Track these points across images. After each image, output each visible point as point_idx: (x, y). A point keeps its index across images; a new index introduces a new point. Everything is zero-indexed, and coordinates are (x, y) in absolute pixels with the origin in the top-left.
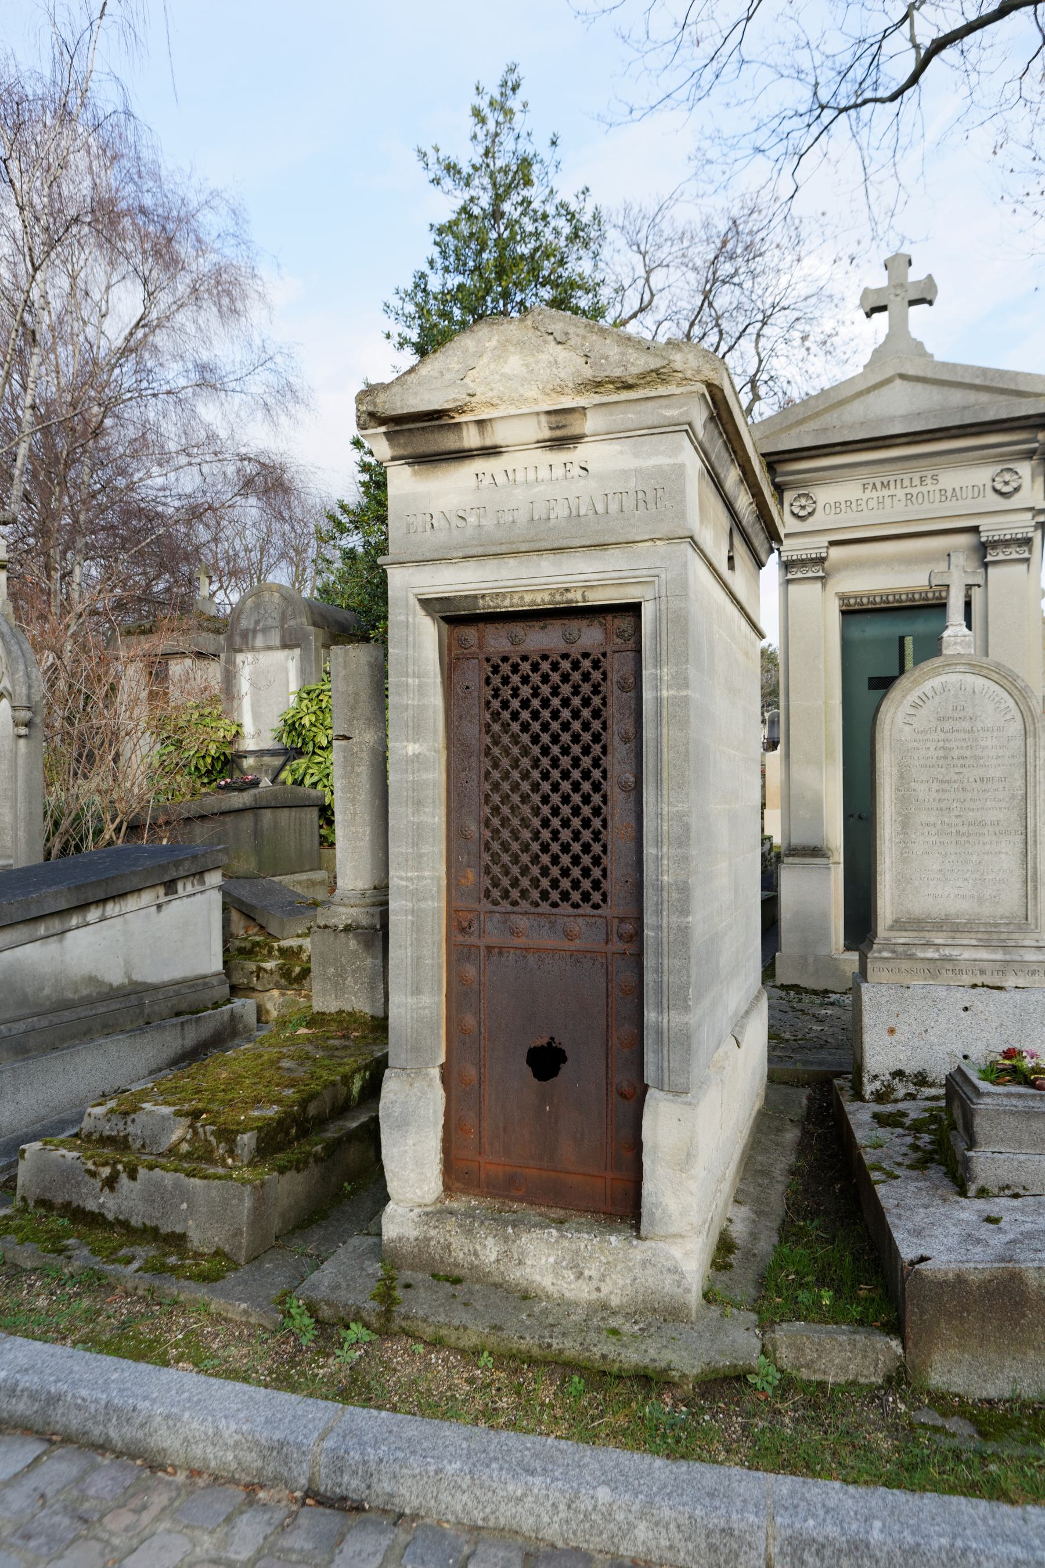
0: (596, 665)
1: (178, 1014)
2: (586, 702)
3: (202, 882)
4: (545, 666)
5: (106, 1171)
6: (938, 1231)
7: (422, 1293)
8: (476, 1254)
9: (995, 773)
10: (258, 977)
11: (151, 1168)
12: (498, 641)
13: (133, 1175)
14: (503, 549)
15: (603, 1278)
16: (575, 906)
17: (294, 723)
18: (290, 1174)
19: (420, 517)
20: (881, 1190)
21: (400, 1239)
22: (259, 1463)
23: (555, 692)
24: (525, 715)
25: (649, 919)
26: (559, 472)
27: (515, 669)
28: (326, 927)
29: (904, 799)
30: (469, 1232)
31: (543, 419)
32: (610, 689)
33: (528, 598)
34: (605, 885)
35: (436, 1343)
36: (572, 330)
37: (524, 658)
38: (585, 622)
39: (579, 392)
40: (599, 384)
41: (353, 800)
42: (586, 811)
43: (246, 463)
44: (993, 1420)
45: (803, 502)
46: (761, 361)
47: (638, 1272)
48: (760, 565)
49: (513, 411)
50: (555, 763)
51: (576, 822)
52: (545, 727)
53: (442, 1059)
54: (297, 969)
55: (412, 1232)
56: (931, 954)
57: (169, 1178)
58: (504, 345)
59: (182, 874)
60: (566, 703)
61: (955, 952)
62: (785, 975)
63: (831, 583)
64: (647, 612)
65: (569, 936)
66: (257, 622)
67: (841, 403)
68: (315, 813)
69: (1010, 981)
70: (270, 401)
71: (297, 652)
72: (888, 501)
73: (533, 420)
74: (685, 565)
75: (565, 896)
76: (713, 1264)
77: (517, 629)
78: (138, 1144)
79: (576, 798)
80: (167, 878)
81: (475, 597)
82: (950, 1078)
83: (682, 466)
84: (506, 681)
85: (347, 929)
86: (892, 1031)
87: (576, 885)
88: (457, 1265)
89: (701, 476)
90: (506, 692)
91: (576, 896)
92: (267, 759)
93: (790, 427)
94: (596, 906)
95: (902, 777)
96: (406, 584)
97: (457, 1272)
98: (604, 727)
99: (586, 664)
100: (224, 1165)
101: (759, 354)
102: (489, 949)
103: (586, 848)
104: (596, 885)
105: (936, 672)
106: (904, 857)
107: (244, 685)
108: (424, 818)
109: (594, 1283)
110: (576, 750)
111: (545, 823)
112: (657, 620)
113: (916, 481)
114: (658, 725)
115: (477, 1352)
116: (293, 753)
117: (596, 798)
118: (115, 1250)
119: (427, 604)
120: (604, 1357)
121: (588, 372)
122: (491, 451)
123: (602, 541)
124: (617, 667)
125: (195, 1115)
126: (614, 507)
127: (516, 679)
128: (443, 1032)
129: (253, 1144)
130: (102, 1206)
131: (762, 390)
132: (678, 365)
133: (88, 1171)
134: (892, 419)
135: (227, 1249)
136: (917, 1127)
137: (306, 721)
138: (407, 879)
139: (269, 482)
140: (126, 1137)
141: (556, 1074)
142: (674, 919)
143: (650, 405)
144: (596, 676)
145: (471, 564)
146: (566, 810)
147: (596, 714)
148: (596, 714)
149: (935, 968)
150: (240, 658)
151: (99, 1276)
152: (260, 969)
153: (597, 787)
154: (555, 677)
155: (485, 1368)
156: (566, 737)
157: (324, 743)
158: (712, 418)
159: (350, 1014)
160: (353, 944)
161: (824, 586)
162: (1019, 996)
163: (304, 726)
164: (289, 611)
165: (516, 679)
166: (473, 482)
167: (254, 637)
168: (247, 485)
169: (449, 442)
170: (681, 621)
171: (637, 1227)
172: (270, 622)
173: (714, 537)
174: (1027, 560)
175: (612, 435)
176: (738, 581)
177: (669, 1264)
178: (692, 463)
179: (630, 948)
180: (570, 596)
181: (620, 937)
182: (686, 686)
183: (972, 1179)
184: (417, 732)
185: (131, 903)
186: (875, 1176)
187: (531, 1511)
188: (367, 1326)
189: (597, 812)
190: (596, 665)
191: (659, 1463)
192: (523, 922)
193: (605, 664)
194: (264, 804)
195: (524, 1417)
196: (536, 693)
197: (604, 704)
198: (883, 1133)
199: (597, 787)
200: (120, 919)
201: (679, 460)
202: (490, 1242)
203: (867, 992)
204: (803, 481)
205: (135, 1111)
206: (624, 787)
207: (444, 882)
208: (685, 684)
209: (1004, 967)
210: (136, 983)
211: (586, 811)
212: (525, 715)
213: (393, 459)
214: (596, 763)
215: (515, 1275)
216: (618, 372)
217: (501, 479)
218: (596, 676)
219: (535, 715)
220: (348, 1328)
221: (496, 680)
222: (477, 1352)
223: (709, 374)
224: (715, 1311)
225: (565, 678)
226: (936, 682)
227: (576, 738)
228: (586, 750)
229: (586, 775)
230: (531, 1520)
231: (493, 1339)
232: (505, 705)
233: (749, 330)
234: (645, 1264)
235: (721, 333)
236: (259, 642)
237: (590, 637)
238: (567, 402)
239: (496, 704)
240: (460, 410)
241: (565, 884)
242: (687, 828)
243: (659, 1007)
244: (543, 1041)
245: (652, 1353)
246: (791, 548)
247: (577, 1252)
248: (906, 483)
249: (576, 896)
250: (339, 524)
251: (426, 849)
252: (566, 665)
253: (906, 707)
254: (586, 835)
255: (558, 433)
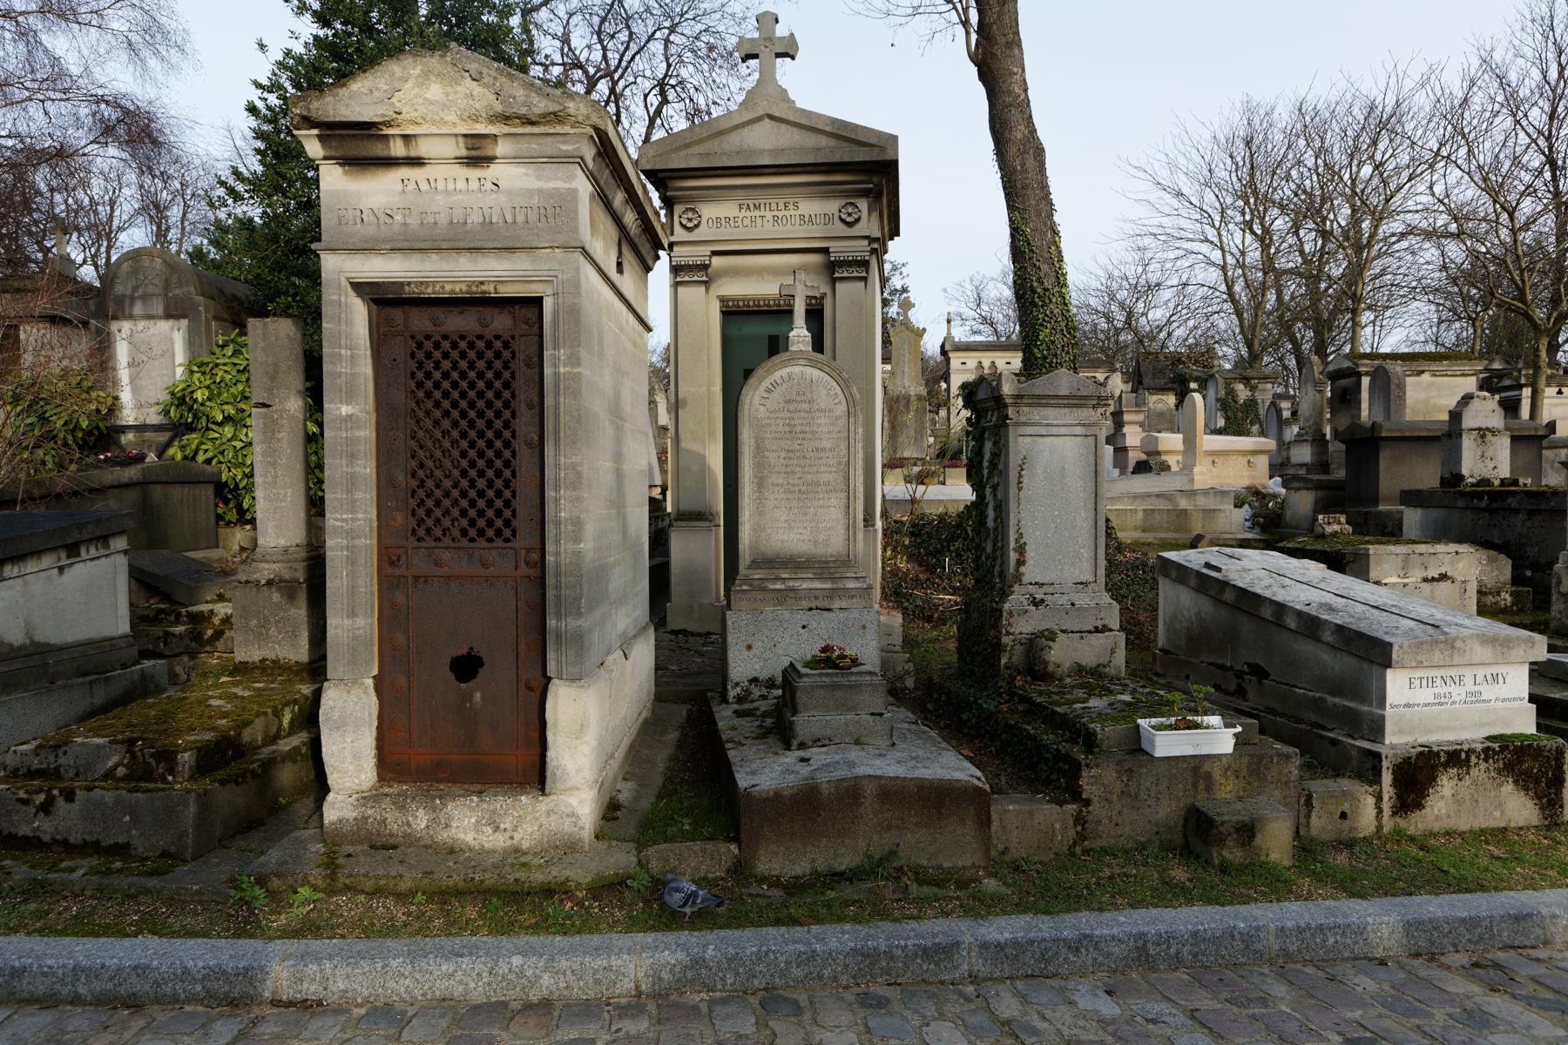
0: (506, 345)
1: (84, 674)
2: (498, 375)
3: (107, 547)
4: (463, 345)
5: (41, 797)
6: (767, 770)
7: (362, 859)
8: (409, 824)
9: (827, 444)
10: (166, 643)
11: (89, 789)
12: (421, 322)
13: (70, 796)
14: (427, 245)
15: (515, 829)
16: (490, 540)
17: (183, 397)
18: (230, 787)
19: (351, 212)
20: (731, 754)
21: (340, 821)
22: (227, 988)
23: (472, 366)
24: (446, 385)
25: (550, 547)
26: (474, 185)
27: (437, 346)
28: (247, 582)
29: (759, 466)
30: (402, 808)
31: (461, 140)
32: (518, 365)
33: (448, 287)
34: (515, 523)
35: (378, 892)
36: (485, 71)
37: (445, 337)
38: (497, 310)
39: (491, 122)
40: (507, 118)
41: (274, 464)
42: (499, 463)
43: (103, 106)
44: (795, 887)
45: (690, 215)
46: (669, 66)
47: (543, 820)
48: (648, 269)
49: (434, 130)
50: (472, 424)
51: (490, 473)
52: (463, 395)
53: (375, 672)
54: (210, 632)
55: (351, 814)
56: (778, 586)
57: (109, 797)
58: (426, 74)
59: (86, 536)
60: (481, 375)
61: (796, 584)
62: (675, 622)
63: (713, 287)
64: (548, 304)
65: (485, 565)
66: (135, 288)
67: (721, 133)
68: (209, 491)
69: (837, 604)
70: (134, 37)
71: (184, 323)
72: (759, 220)
73: (453, 140)
74: (577, 270)
75: (481, 533)
76: (604, 818)
77: (439, 312)
78: (71, 773)
79: (490, 454)
80: (69, 541)
81: (402, 284)
82: (785, 672)
83: (575, 190)
84: (429, 355)
85: (269, 583)
86: (749, 647)
87: (490, 523)
88: (391, 835)
89: (592, 197)
90: (429, 365)
91: (490, 533)
92: (149, 435)
93: (678, 149)
94: (507, 540)
95: (758, 447)
96: (337, 267)
97: (392, 841)
98: (513, 397)
99: (498, 344)
100: (165, 781)
101: (667, 59)
102: (416, 578)
103: (499, 494)
104: (507, 523)
105: (784, 365)
106: (759, 512)
107: (122, 352)
108: (357, 469)
109: (508, 834)
110: (490, 414)
111: (464, 474)
112: (556, 312)
113: (781, 206)
114: (557, 395)
115: (413, 893)
116: (178, 429)
117: (507, 454)
118: (55, 864)
119: (359, 288)
120: (516, 880)
121: (499, 107)
122: (416, 162)
123: (510, 245)
124: (523, 347)
125: (131, 742)
126: (520, 219)
127: (437, 355)
128: (376, 649)
129: (193, 762)
130: (38, 828)
131: (671, 95)
132: (572, 111)
133: (21, 801)
134: (762, 152)
135: (173, 849)
136: (765, 715)
137: (199, 395)
138: (342, 520)
139: (137, 131)
140: (57, 768)
141: (452, 669)
142: (570, 546)
143: (549, 140)
144: (506, 354)
145: (398, 256)
146: (481, 463)
147: (507, 385)
148: (507, 385)
149: (782, 597)
150: (114, 326)
151: (42, 884)
152: (168, 634)
153: (507, 444)
154: (472, 354)
155: (420, 903)
156: (481, 404)
157: (220, 418)
158: (599, 154)
159: (274, 662)
160: (276, 597)
161: (707, 290)
162: (842, 615)
163: (196, 400)
164: (174, 279)
165: (437, 355)
166: (399, 186)
167: (132, 304)
168: (106, 131)
169: (378, 150)
170: (575, 314)
171: (543, 791)
172: (151, 289)
173: (604, 248)
174: (865, 279)
175: (519, 159)
176: (627, 283)
177: (568, 811)
178: (584, 187)
179: (534, 572)
180: (484, 288)
181: (527, 564)
182: (579, 364)
183: (794, 737)
184: (350, 396)
185: (31, 566)
186: (729, 745)
187: (461, 982)
188: (315, 888)
189: (507, 464)
190: (506, 345)
191: (558, 938)
192: (446, 555)
193: (514, 345)
194: (153, 478)
195: (454, 926)
196: (455, 367)
197: (513, 377)
198: (737, 721)
199: (507, 444)
200: (19, 581)
201: (574, 185)
202: (421, 813)
203: (731, 617)
204: (690, 197)
205: (66, 744)
206: (529, 444)
207: (375, 524)
208: (578, 363)
209: (832, 593)
210: (38, 644)
211: (499, 463)
212: (446, 385)
213: (325, 158)
214: (507, 425)
215: (443, 836)
216: (523, 110)
217: (424, 186)
218: (506, 354)
219: (455, 385)
220: (296, 892)
221: (420, 355)
222: (413, 893)
223: (595, 120)
224: (603, 845)
225: (480, 355)
226: (784, 372)
227: (489, 405)
228: (498, 415)
229: (498, 435)
230: (461, 988)
231: (425, 881)
232: (428, 376)
233: (658, 35)
234: (548, 813)
235: (631, 34)
236: (138, 309)
237: (501, 322)
238: (481, 129)
239: (420, 375)
240: (388, 124)
241: (481, 523)
242: (579, 475)
243: (559, 616)
244: (464, 651)
245: (554, 873)
246: (684, 254)
247: (494, 812)
248: (774, 206)
249: (490, 533)
250: (232, 192)
251: (359, 495)
252: (481, 345)
253: (761, 392)
254: (499, 483)
255: (474, 153)
